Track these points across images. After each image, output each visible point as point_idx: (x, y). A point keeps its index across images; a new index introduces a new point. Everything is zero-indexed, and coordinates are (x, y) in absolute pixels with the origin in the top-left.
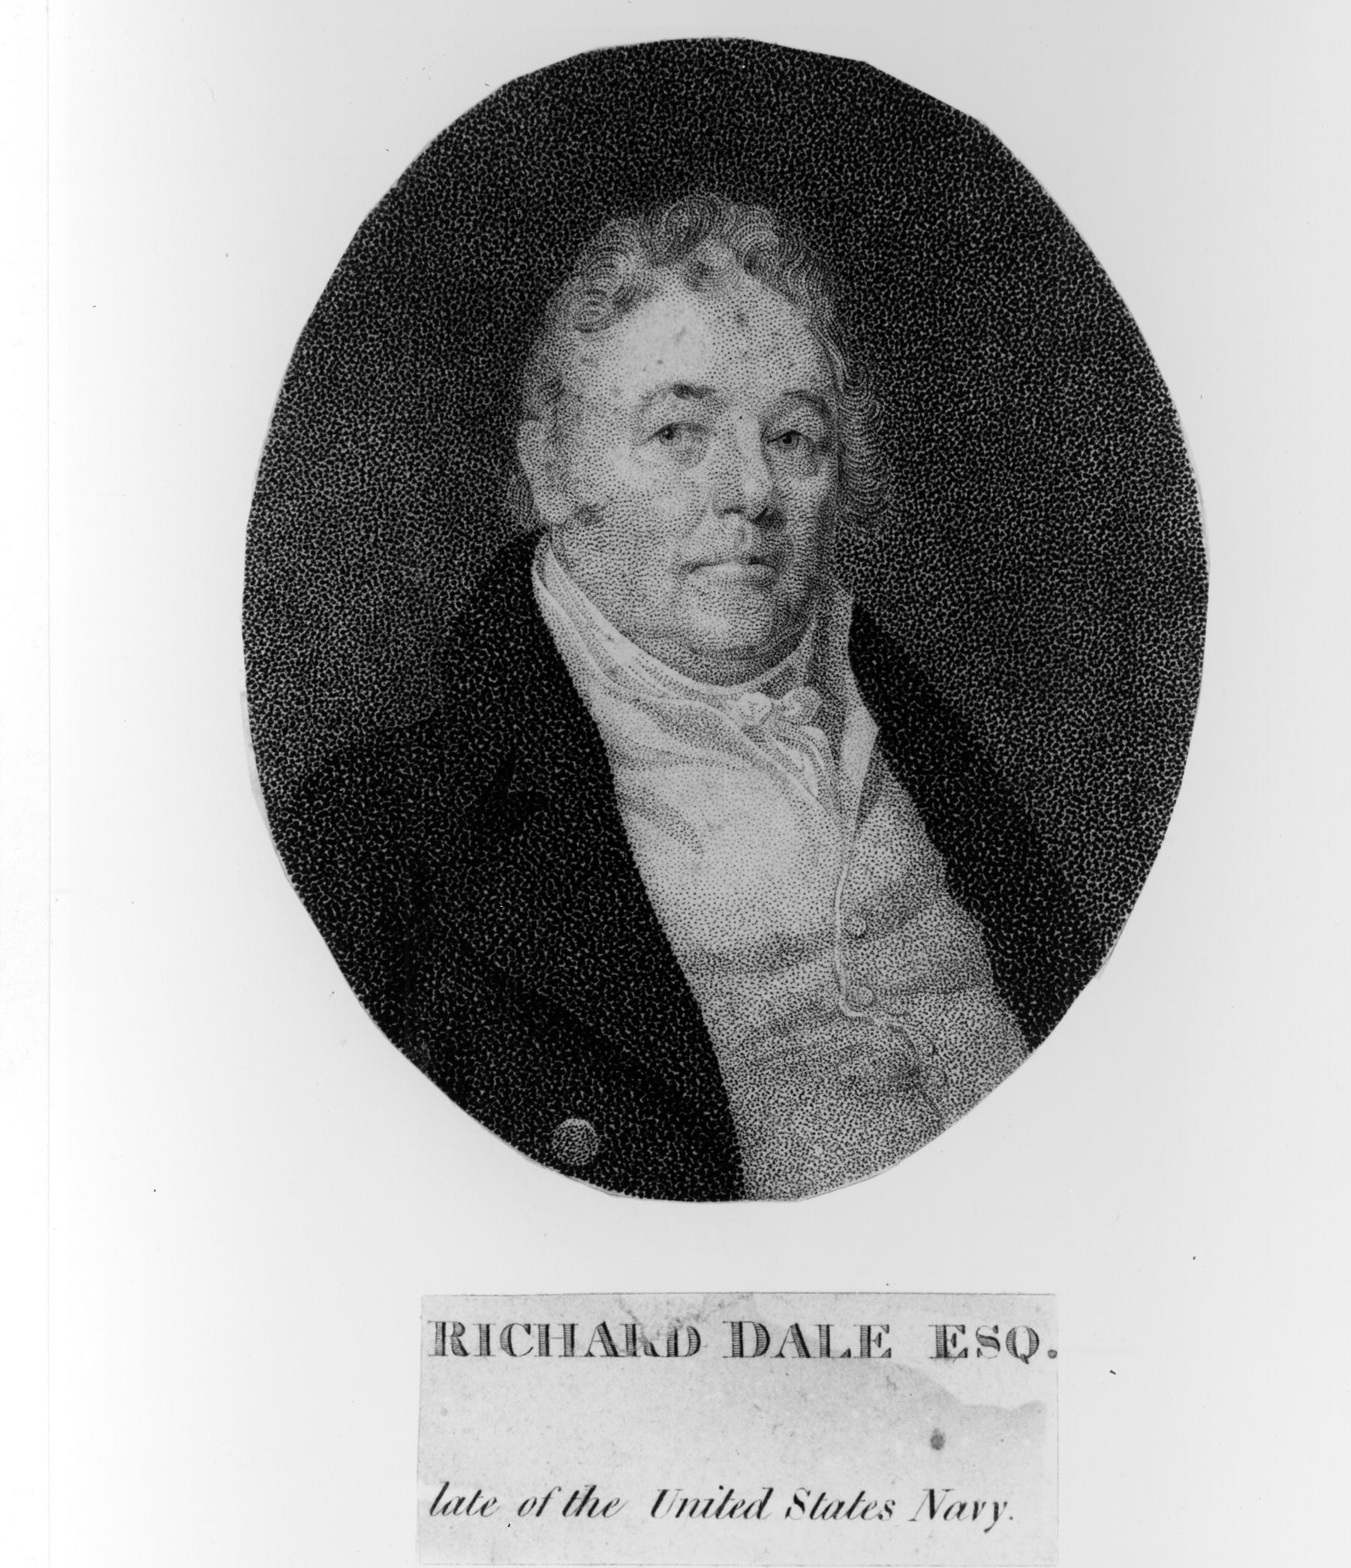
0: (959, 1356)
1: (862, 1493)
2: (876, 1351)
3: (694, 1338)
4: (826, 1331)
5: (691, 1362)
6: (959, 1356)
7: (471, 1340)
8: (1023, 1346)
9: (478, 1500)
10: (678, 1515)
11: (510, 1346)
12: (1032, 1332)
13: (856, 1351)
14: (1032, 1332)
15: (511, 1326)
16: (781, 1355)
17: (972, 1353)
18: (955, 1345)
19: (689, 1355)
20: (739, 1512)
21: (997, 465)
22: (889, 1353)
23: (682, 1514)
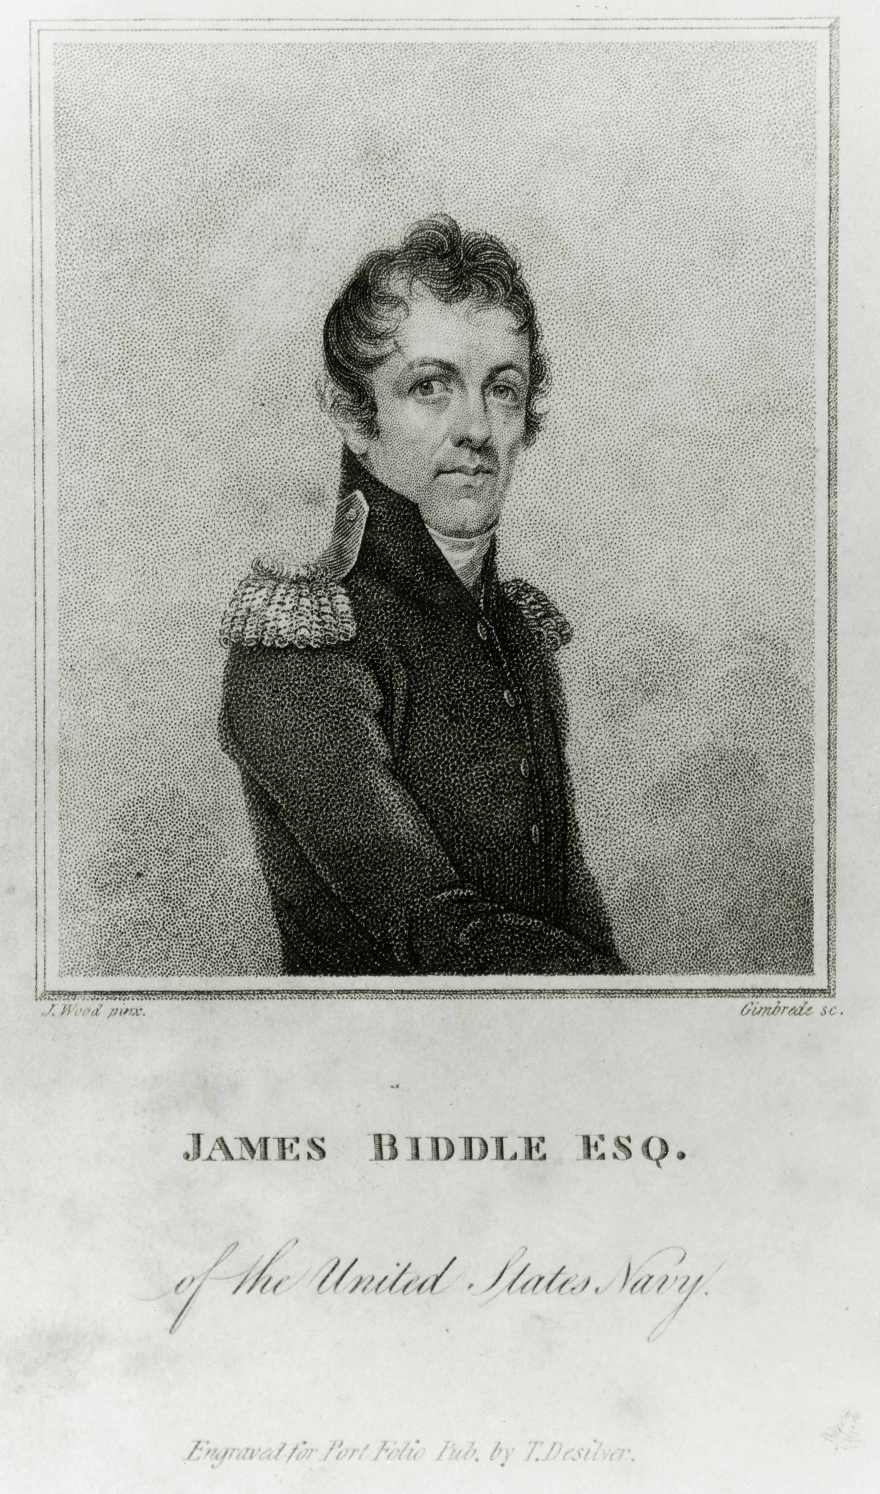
0: (540, 1159)
1: (564, 1267)
2: (594, 1153)
3: (450, 1146)
4: (500, 1141)
5: (394, 1162)
6: (540, 1159)
7: (273, 1148)
8: (655, 1149)
9: (404, 1276)
10: (249, 1291)
11: (648, 1151)
12: (663, 1142)
13: (521, 1154)
14: (663, 1142)
15: (649, 1141)
16: (210, 1158)
17: (609, 1156)
18: (291, 1152)
19: (479, 1159)
20: (269, 1286)
21: (463, 770)
22: (544, 1157)
23: (239, 1291)
